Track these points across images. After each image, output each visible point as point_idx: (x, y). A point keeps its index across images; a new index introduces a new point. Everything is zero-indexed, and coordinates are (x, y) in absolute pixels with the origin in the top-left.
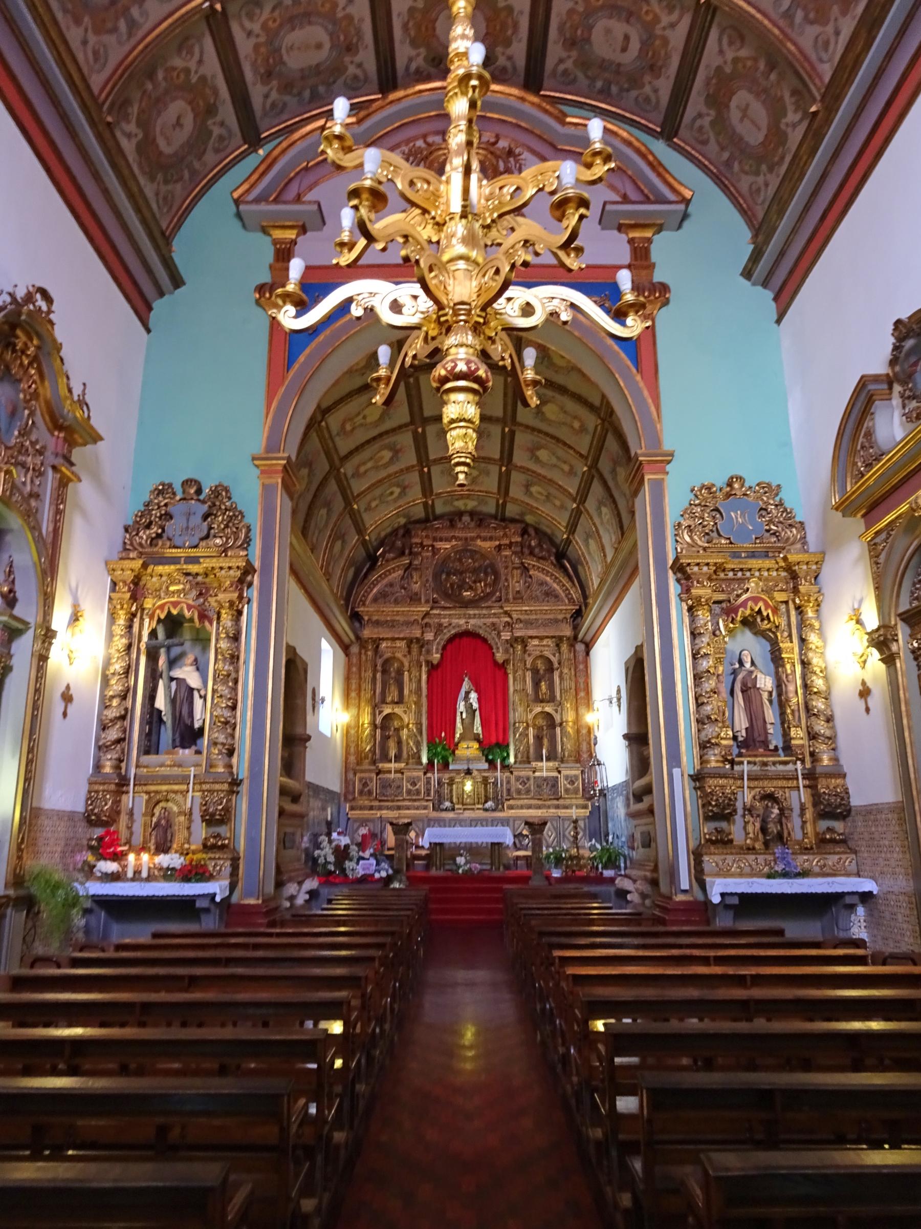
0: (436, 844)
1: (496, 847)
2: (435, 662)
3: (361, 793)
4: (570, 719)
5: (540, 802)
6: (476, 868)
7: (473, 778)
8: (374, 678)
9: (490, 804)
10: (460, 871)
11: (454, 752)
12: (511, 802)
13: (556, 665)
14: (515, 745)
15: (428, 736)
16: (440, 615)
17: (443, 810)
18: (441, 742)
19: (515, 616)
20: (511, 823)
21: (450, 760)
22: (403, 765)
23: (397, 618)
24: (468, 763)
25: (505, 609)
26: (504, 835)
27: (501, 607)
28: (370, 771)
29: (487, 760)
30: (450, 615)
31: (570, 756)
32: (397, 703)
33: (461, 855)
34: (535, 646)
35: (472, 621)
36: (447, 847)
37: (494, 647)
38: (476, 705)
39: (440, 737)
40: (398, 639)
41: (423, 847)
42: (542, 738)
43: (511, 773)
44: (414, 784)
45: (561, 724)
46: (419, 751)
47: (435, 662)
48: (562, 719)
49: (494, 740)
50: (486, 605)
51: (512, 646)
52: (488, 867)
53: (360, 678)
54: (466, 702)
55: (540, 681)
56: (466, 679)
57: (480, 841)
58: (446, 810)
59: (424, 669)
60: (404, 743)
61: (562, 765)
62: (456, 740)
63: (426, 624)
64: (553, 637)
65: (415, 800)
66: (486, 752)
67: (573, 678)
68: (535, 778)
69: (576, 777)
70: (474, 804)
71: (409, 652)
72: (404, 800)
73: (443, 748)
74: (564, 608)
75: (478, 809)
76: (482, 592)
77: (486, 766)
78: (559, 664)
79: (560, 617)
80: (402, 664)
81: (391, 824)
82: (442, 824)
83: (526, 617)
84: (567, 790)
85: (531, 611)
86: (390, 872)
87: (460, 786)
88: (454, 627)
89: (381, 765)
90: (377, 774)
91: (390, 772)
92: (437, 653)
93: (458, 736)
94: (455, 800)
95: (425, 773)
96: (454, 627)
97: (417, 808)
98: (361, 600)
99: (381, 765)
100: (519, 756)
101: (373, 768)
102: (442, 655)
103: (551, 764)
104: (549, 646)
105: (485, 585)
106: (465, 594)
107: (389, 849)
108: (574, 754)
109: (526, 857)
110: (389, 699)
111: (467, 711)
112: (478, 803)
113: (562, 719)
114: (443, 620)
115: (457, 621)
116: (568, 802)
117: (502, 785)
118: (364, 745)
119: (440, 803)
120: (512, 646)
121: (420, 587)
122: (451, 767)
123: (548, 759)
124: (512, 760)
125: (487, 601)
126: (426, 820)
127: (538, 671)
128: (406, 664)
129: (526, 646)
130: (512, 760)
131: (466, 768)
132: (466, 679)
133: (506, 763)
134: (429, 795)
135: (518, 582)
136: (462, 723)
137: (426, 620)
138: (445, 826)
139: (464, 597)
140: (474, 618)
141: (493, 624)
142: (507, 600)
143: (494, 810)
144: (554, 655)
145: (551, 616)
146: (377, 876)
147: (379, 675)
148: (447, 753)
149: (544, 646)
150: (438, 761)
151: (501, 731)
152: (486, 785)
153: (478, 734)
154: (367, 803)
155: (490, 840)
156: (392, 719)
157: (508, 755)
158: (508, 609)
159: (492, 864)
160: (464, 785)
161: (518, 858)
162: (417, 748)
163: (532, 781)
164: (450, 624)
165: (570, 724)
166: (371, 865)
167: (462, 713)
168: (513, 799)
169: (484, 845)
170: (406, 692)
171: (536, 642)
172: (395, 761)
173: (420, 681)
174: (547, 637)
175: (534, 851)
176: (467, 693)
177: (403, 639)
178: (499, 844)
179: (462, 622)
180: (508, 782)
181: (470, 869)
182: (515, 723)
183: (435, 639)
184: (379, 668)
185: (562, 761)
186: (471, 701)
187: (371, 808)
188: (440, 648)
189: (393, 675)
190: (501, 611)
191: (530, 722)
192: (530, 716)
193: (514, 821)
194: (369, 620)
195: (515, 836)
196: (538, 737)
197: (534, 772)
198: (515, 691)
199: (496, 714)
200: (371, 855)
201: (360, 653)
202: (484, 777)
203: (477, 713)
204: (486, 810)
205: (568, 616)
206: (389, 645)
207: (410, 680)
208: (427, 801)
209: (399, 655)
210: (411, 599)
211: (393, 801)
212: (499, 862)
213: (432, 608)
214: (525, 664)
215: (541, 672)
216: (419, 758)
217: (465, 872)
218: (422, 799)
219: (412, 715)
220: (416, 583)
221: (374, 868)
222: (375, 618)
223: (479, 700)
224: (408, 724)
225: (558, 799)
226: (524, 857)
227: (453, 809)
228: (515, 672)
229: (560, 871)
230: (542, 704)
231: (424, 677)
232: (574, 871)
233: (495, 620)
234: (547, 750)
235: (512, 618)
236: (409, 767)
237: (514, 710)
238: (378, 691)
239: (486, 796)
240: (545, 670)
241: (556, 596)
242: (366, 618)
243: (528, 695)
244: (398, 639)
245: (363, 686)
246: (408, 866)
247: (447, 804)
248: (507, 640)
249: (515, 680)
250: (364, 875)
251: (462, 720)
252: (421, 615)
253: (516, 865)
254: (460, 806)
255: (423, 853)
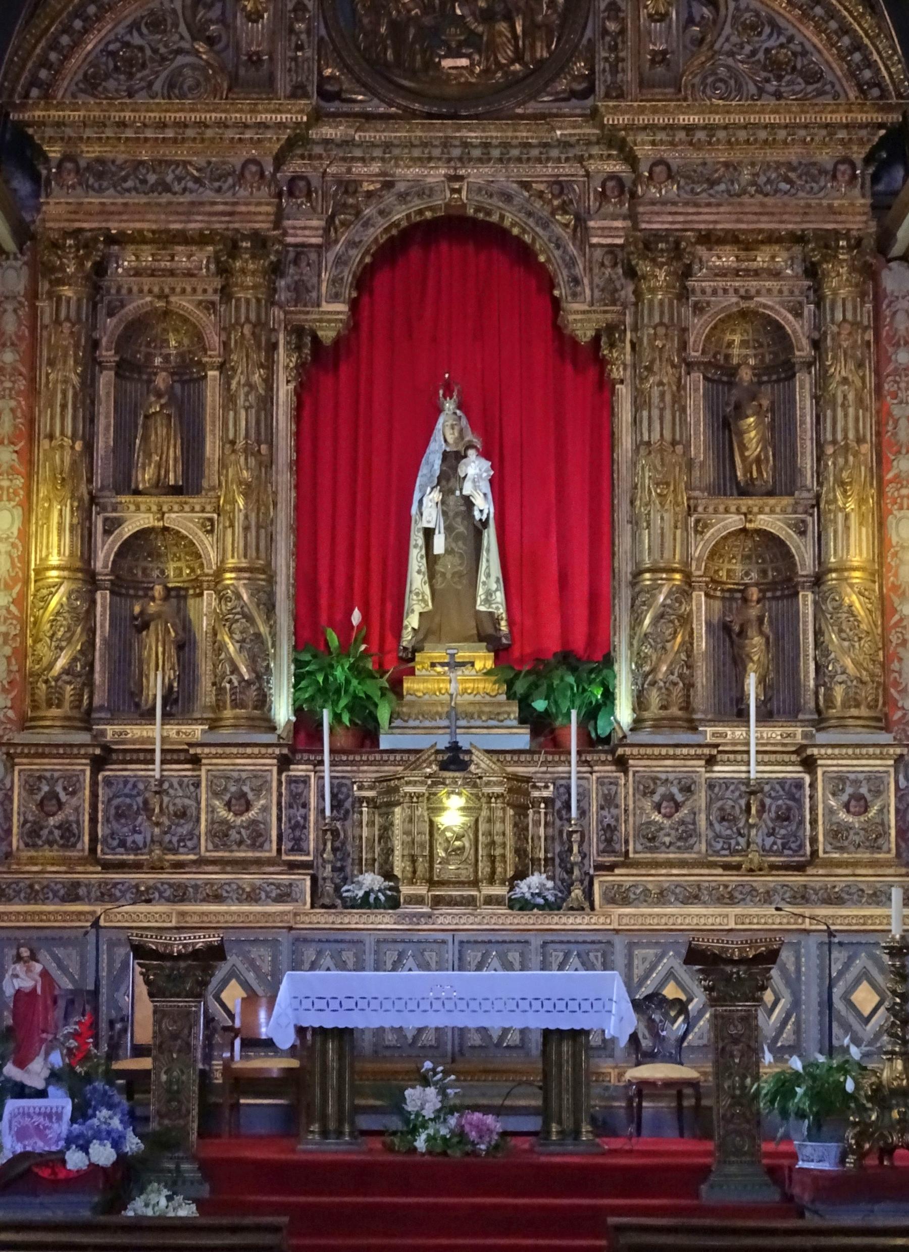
0: (322, 1032)
1: (566, 1047)
2: (327, 335)
3: (33, 834)
4: (856, 560)
5: (732, 879)
6: (483, 1131)
7: (473, 783)
8: (88, 385)
9: (535, 881)
10: (421, 1143)
11: (396, 686)
12: (622, 877)
13: (804, 351)
14: (640, 659)
15: (297, 619)
16: (347, 143)
17: (352, 904)
18: (345, 648)
19: (644, 151)
20: (619, 958)
21: (383, 714)
22: (197, 731)
23: (181, 153)
24: (452, 729)
25: (608, 120)
26: (598, 1003)
27: (594, 115)
28: (68, 751)
29: (527, 717)
30: (388, 146)
31: (852, 701)
32: (176, 490)
33: (425, 1081)
34: (722, 273)
35: (476, 174)
36: (366, 1044)
37: (562, 276)
38: (484, 506)
39: (345, 629)
40: (183, 238)
41: (269, 1044)
42: (742, 633)
43: (622, 763)
44: (241, 803)
45: (818, 581)
46: (261, 676)
47: (327, 335)
48: (820, 559)
49: (553, 645)
50: (532, 107)
51: (631, 273)
52: (533, 1124)
53: (33, 391)
54: (447, 492)
55: (739, 411)
56: (449, 405)
57: (495, 1023)
58: (365, 903)
59: (284, 358)
60: (204, 644)
61: (821, 738)
62: (407, 638)
63: (292, 181)
64: (798, 239)
65: (243, 865)
66: (520, 687)
67: (869, 399)
68: (711, 786)
69: (876, 783)
70: (475, 883)
71: (225, 293)
72: (202, 862)
73: (357, 670)
74: (841, 117)
75: (490, 900)
76: (518, 57)
77: (521, 738)
78: (816, 344)
79: (826, 157)
80: (198, 336)
81: (140, 951)
82: (348, 956)
83: (695, 156)
84: (837, 833)
85: (711, 129)
86: (133, 1144)
87: (421, 811)
88: (403, 197)
89: (110, 731)
90: (98, 764)
91: (145, 756)
92: (335, 297)
93: (412, 621)
94: (399, 866)
95: (284, 763)
96: (403, 197)
97: (252, 897)
98: (34, 82)
99: (110, 731)
100: (654, 698)
101: (84, 737)
102: (354, 305)
103: (775, 733)
104: (776, 274)
105: (531, 29)
106: (447, 63)
107: (139, 1051)
108: (867, 693)
109: (676, 1087)
110: (146, 476)
111: (449, 529)
112: (491, 881)
113: (820, 559)
114: (359, 169)
115: (414, 171)
116: (840, 879)
117: (583, 813)
118: (44, 650)
119: (343, 875)
120: (631, 273)
121: (273, 35)
122: (385, 743)
123: (766, 716)
124: (624, 713)
125: (533, 97)
126: (284, 938)
127: (732, 372)
128: (214, 339)
129: (687, 272)
130: (624, 713)
131: (443, 742)
132: (449, 405)
133: (603, 728)
134: (298, 848)
135: (663, 17)
136: (432, 575)
137: (294, 167)
138: (360, 966)
139: (444, 78)
140: (484, 160)
141: (560, 186)
142: (617, 93)
143: (550, 907)
144: (798, 314)
145: (793, 154)
146: (75, 1160)
147: (106, 380)
148: (372, 688)
149: (757, 273)
150: (337, 717)
151: (580, 612)
152: (521, 810)
153: (494, 619)
154: (58, 874)
155: (538, 1022)
156: (155, 555)
157: (609, 696)
158: (622, 120)
159: (545, 1112)
160: (437, 810)
161: (644, 1088)
162: (253, 661)
163: (701, 798)
164: (388, 185)
165: (857, 577)
166: (53, 1116)
167: (429, 534)
168: (627, 863)
169: (513, 1039)
170: (212, 448)
171: (726, 258)
172: (166, 716)
173: (266, 402)
174: (772, 238)
175: (722, 1068)
176: (453, 459)
177: (202, 240)
178: (577, 1035)
179: (436, 174)
180: (609, 801)
181: (460, 1134)
182: (637, 574)
183: (329, 243)
184: (107, 354)
185: (820, 722)
186: (468, 489)
187: (72, 894)
188: (348, 276)
189: (161, 381)
190: (591, 131)
191: (697, 571)
192: (699, 549)
193: (631, 946)
194: (67, 157)
195: (637, 1005)
196: (726, 628)
197: (711, 761)
198: (641, 445)
199: (563, 540)
200: (54, 1076)
201: (33, 295)
202: (515, 777)
203: (490, 537)
204: (523, 905)
205: (858, 154)
206: (148, 260)
207: (229, 400)
208: (293, 866)
209: (184, 303)
210: (235, 82)
211: (156, 867)
212: (576, 1109)
213: (317, 117)
214: (683, 346)
215: (746, 375)
216: (263, 702)
217: (436, 1143)
218: (270, 862)
219: (233, 538)
220: (254, 17)
221: (63, 1127)
222: (90, 152)
223: (498, 486)
224: (221, 571)
225: (800, 868)
226: (669, 1084)
227: (394, 903)
228: (642, 371)
229: (833, 1148)
230: (746, 503)
231: (284, 391)
232: (888, 1151)
233: (567, 169)
234: (761, 680)
235: (632, 160)
236: (224, 735)
237: (634, 522)
238: (104, 441)
239: (520, 852)
240: (761, 371)
241: (813, 76)
242: (54, 152)
243: (690, 464)
244: (183, 238)
245: (44, 423)
246: (208, 1113)
247: (371, 880)
248: (611, 249)
249: (640, 402)
250: (25, 1156)
251: (431, 558)
252: (274, 142)
253: (635, 1116)
254: (421, 890)
255: (274, 1065)
